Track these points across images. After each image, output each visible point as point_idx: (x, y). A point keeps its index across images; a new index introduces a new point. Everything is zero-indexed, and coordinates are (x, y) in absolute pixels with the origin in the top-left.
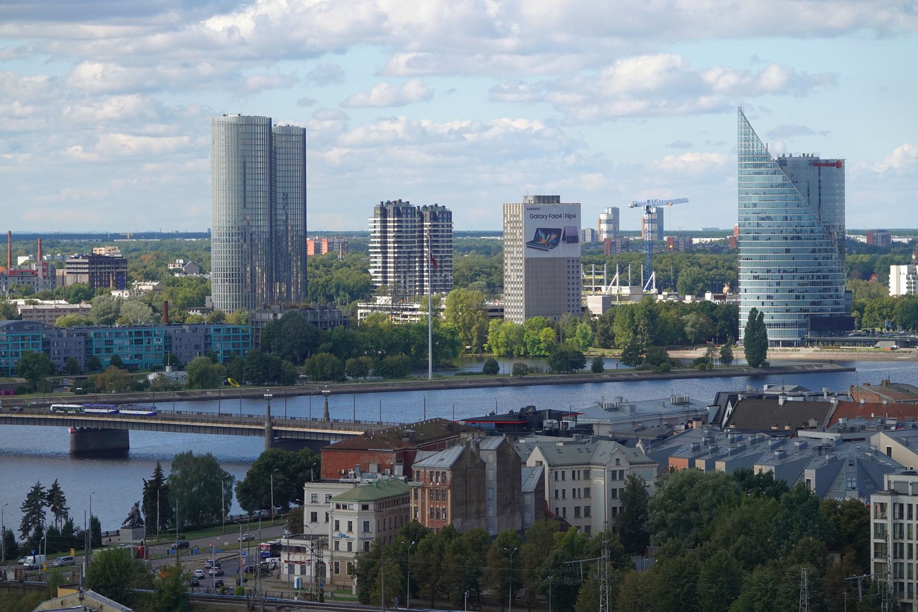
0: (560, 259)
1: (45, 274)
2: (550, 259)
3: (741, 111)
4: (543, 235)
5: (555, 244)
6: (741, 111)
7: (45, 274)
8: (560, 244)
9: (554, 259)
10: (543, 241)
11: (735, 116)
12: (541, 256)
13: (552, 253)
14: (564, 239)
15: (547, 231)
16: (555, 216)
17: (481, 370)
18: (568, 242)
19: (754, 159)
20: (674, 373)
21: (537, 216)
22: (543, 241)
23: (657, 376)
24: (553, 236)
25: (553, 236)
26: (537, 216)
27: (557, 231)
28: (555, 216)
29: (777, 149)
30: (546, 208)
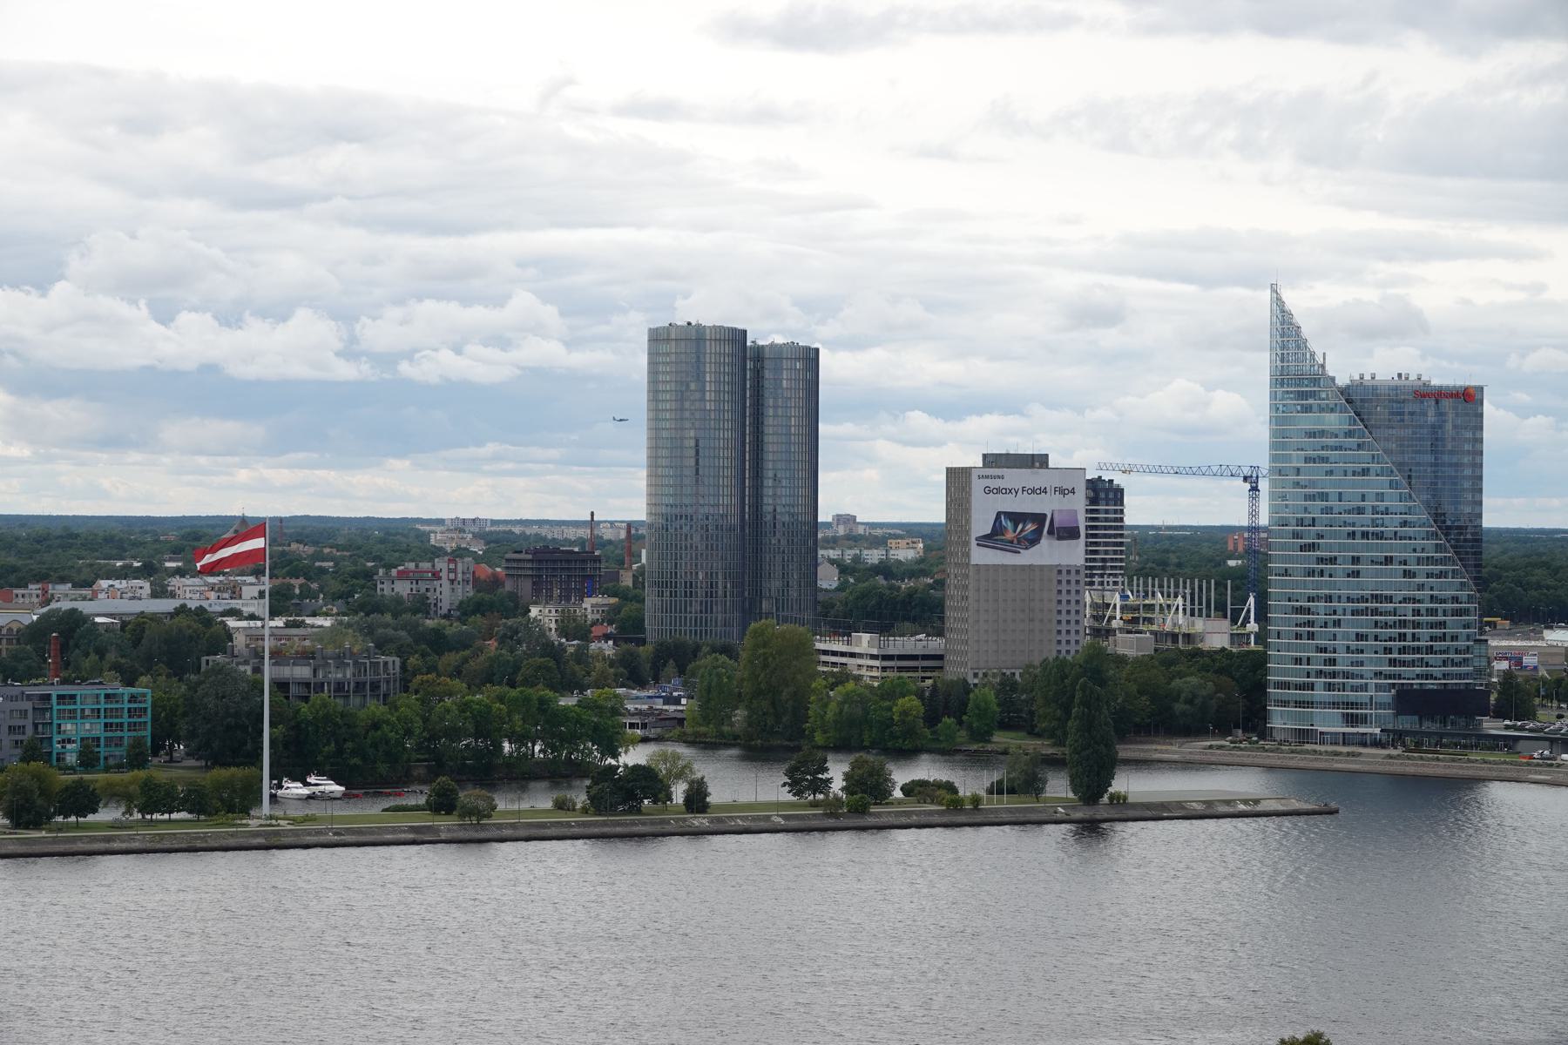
0: (1042, 567)
1: (452, 576)
2: (1023, 568)
3: (1274, 289)
4: (1009, 525)
5: (1034, 540)
6: (1274, 289)
7: (452, 576)
8: (1045, 541)
9: (1031, 568)
10: (1010, 535)
11: (1267, 295)
12: (1006, 562)
13: (1027, 557)
14: (1050, 532)
15: (1017, 518)
16: (1034, 491)
17: (422, 800)
18: (1059, 538)
19: (1298, 381)
20: (878, 815)
21: (999, 491)
22: (1010, 535)
23: (831, 822)
24: (1030, 527)
25: (1030, 527)
26: (999, 491)
27: (1039, 518)
28: (1034, 491)
29: (1343, 368)
30: (1015, 477)
